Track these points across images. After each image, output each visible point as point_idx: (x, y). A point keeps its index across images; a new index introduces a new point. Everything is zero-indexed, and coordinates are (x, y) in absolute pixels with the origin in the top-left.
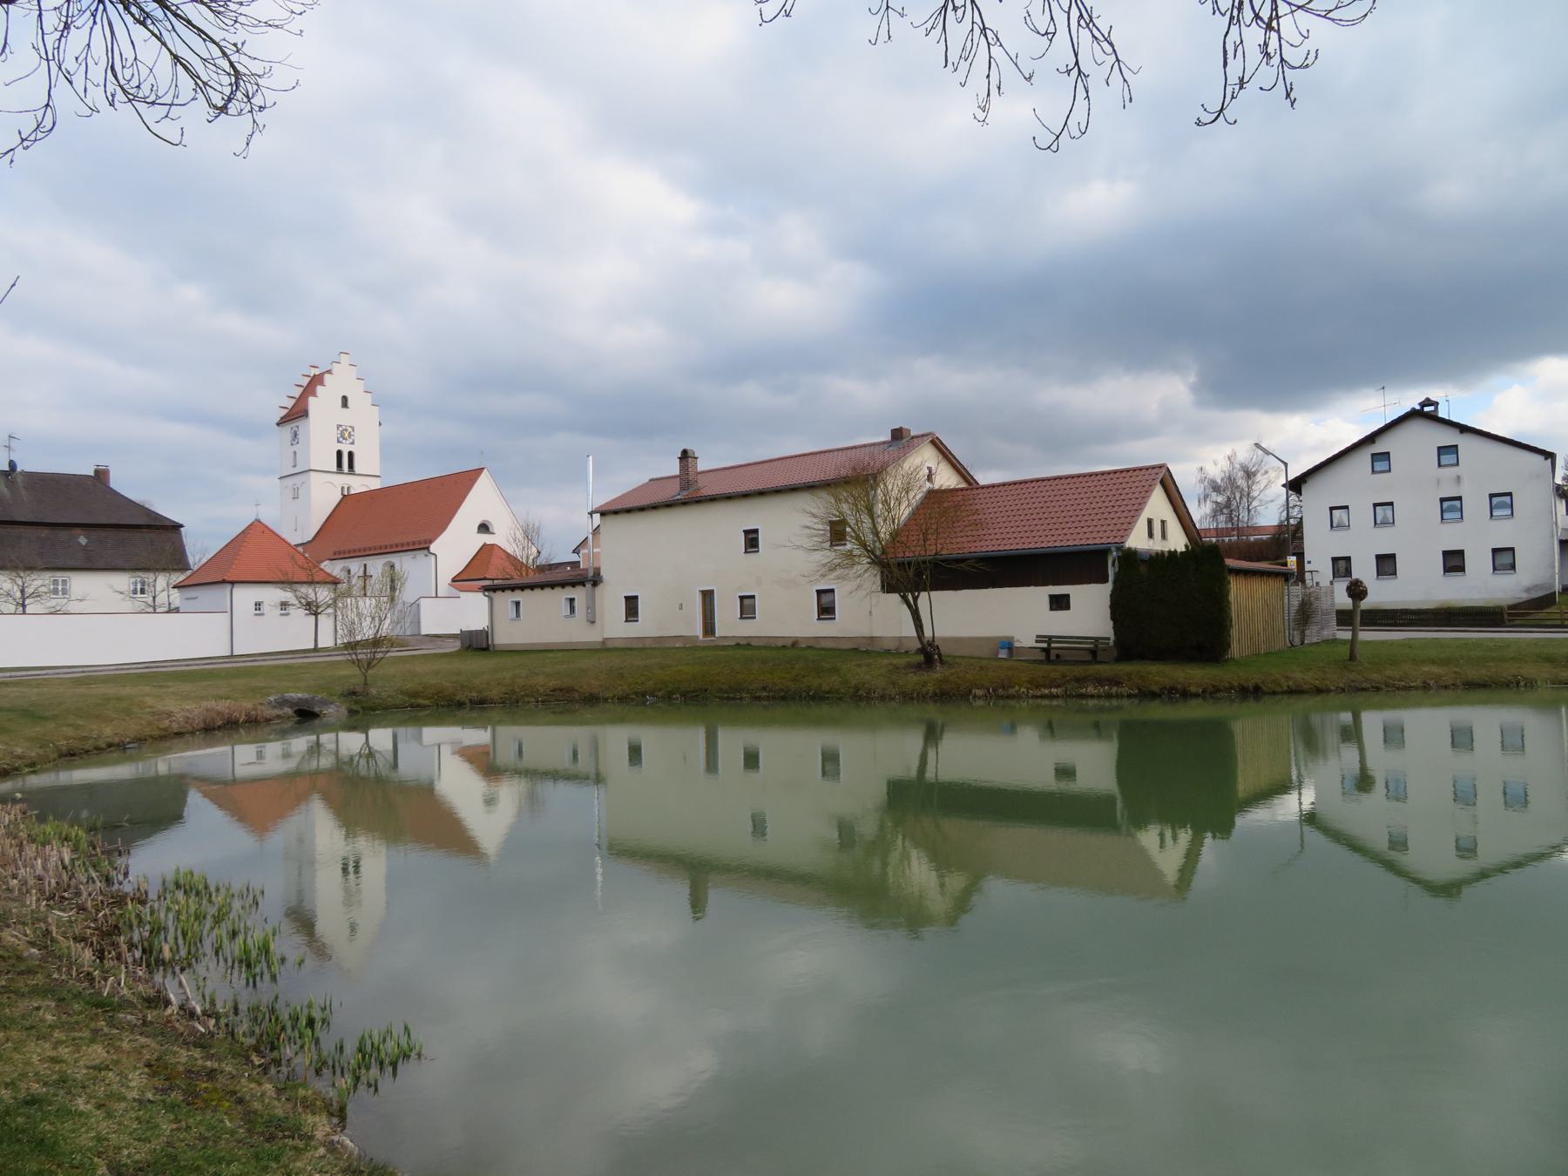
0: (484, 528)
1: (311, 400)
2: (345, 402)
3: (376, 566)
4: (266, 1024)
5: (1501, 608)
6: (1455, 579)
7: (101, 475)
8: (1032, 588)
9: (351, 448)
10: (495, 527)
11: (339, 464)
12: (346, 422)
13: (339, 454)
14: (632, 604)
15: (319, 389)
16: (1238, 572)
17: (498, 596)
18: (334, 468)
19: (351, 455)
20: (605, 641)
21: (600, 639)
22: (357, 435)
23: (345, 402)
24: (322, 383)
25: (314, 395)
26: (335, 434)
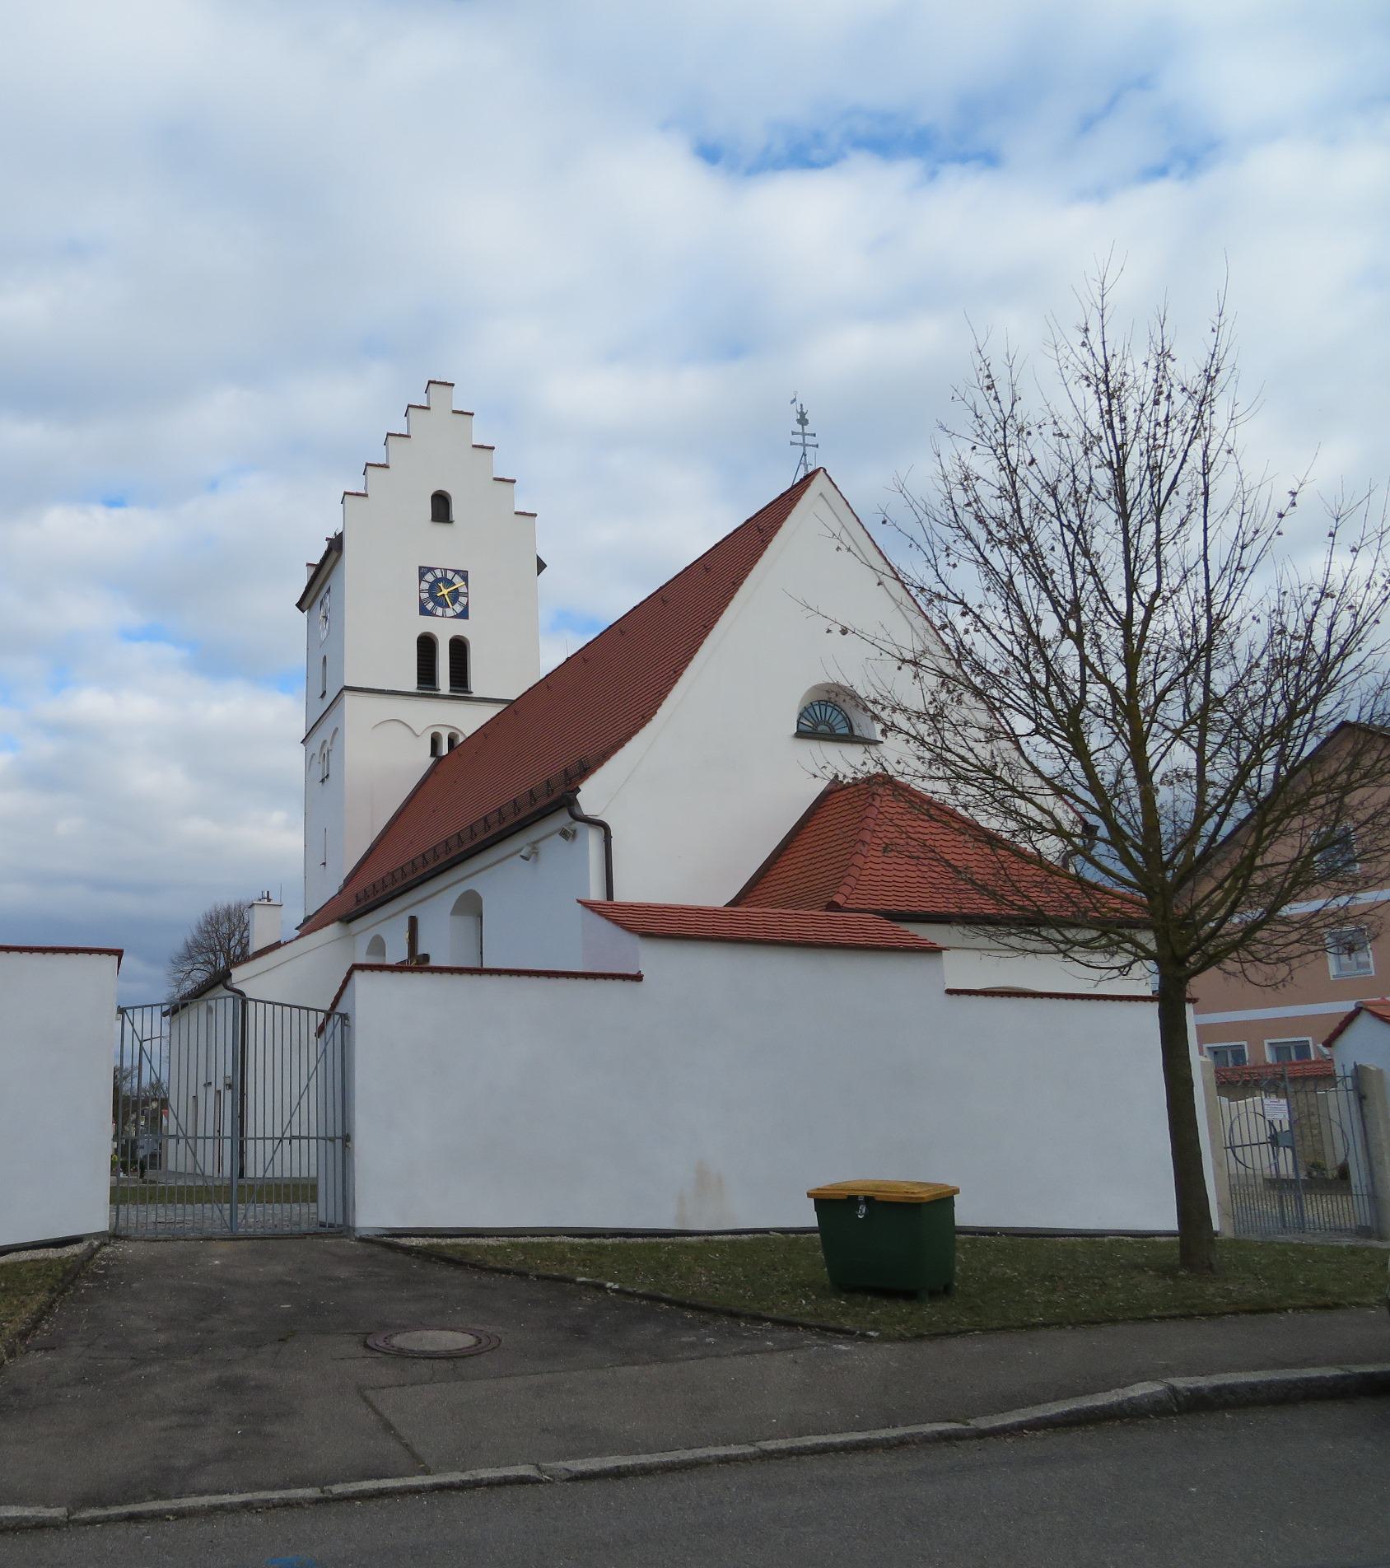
2: (441, 507)
7: (944, 1202)
12: (445, 560)
13: (426, 645)
18: (411, 683)
19: (459, 648)
22: (477, 595)
23: (441, 507)
26: (412, 591)
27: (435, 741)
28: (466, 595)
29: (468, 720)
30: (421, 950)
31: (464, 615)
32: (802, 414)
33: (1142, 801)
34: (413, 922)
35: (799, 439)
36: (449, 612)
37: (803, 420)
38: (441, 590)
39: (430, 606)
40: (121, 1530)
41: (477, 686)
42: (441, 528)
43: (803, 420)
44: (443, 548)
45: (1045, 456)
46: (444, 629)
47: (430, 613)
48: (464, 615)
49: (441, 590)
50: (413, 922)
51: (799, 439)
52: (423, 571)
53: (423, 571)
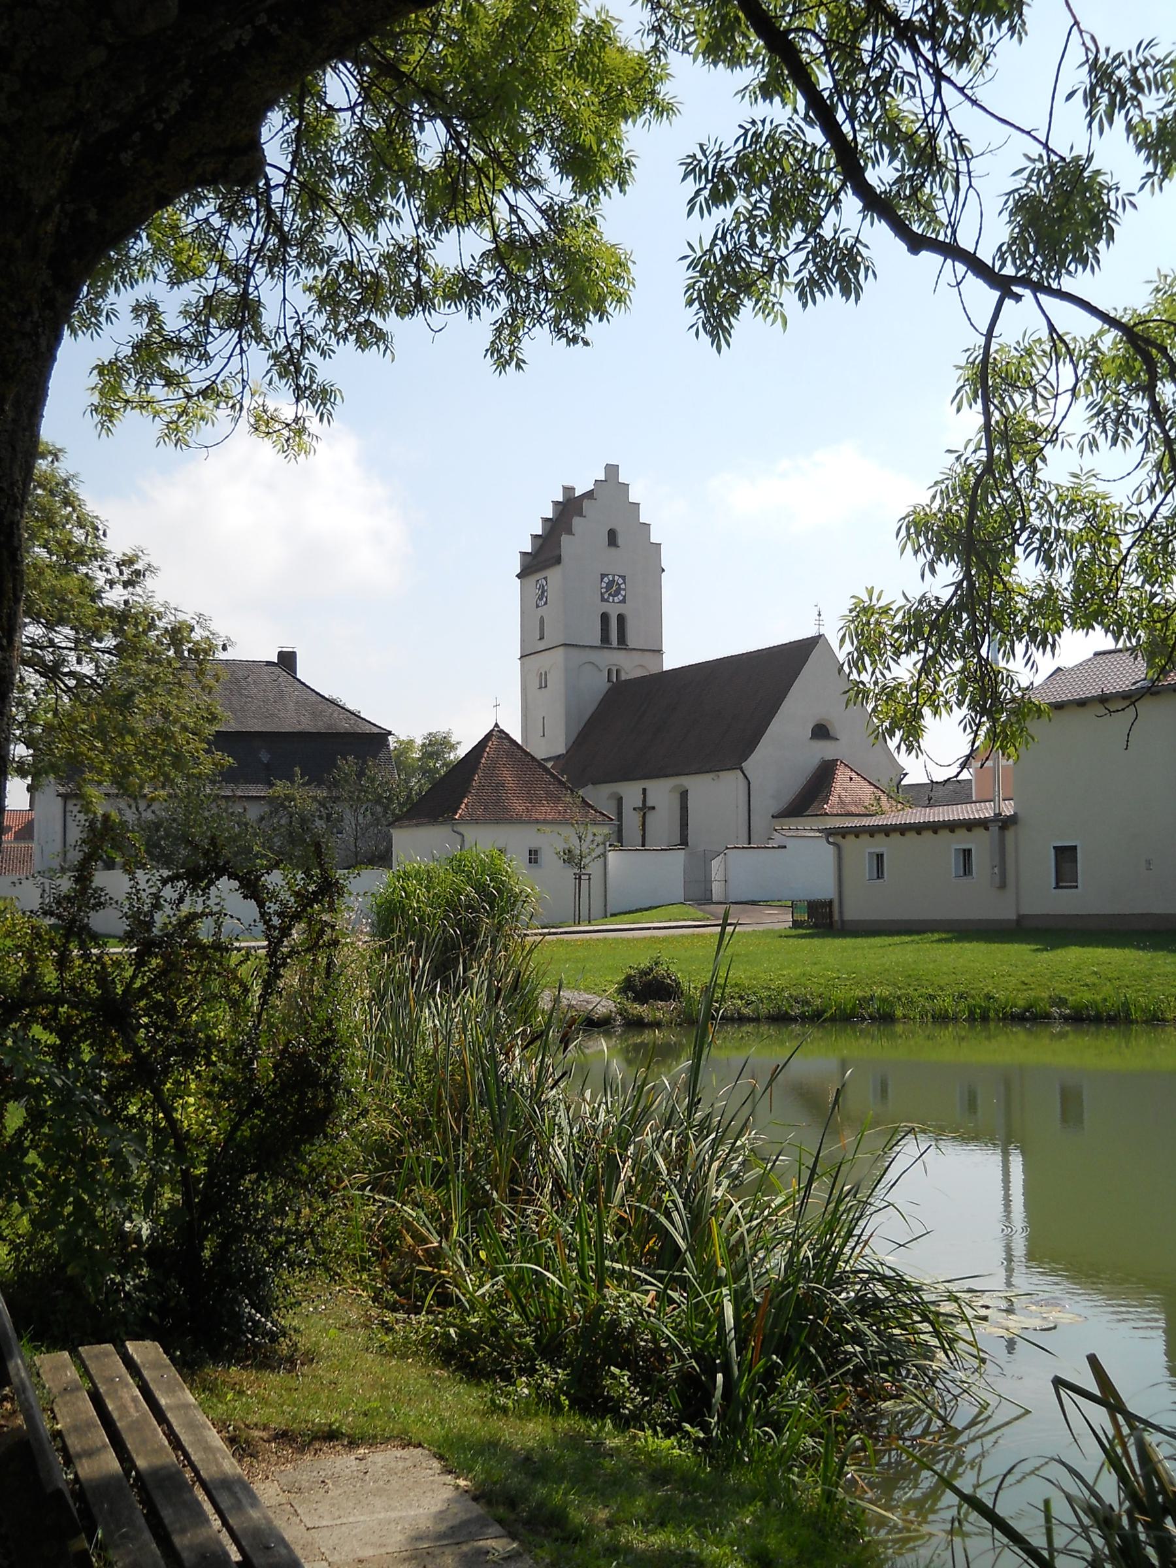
0: (821, 732)
1: (565, 539)
3: (661, 792)
4: (606, 1534)
5: (371, 741)
6: (534, 846)
8: (972, 918)
9: (621, 608)
10: (836, 729)
11: (605, 639)
13: (605, 618)
14: (1066, 856)
15: (577, 521)
16: (841, 913)
17: (849, 843)
18: (598, 643)
19: (621, 619)
20: (1021, 918)
21: (1013, 916)
24: (580, 514)
25: (570, 532)
27: (609, 671)
30: (649, 803)
34: (644, 790)
38: (612, 588)
41: (632, 641)
42: (613, 549)
44: (615, 562)
46: (614, 611)
48: (624, 601)
49: (612, 588)
53: (603, 576)
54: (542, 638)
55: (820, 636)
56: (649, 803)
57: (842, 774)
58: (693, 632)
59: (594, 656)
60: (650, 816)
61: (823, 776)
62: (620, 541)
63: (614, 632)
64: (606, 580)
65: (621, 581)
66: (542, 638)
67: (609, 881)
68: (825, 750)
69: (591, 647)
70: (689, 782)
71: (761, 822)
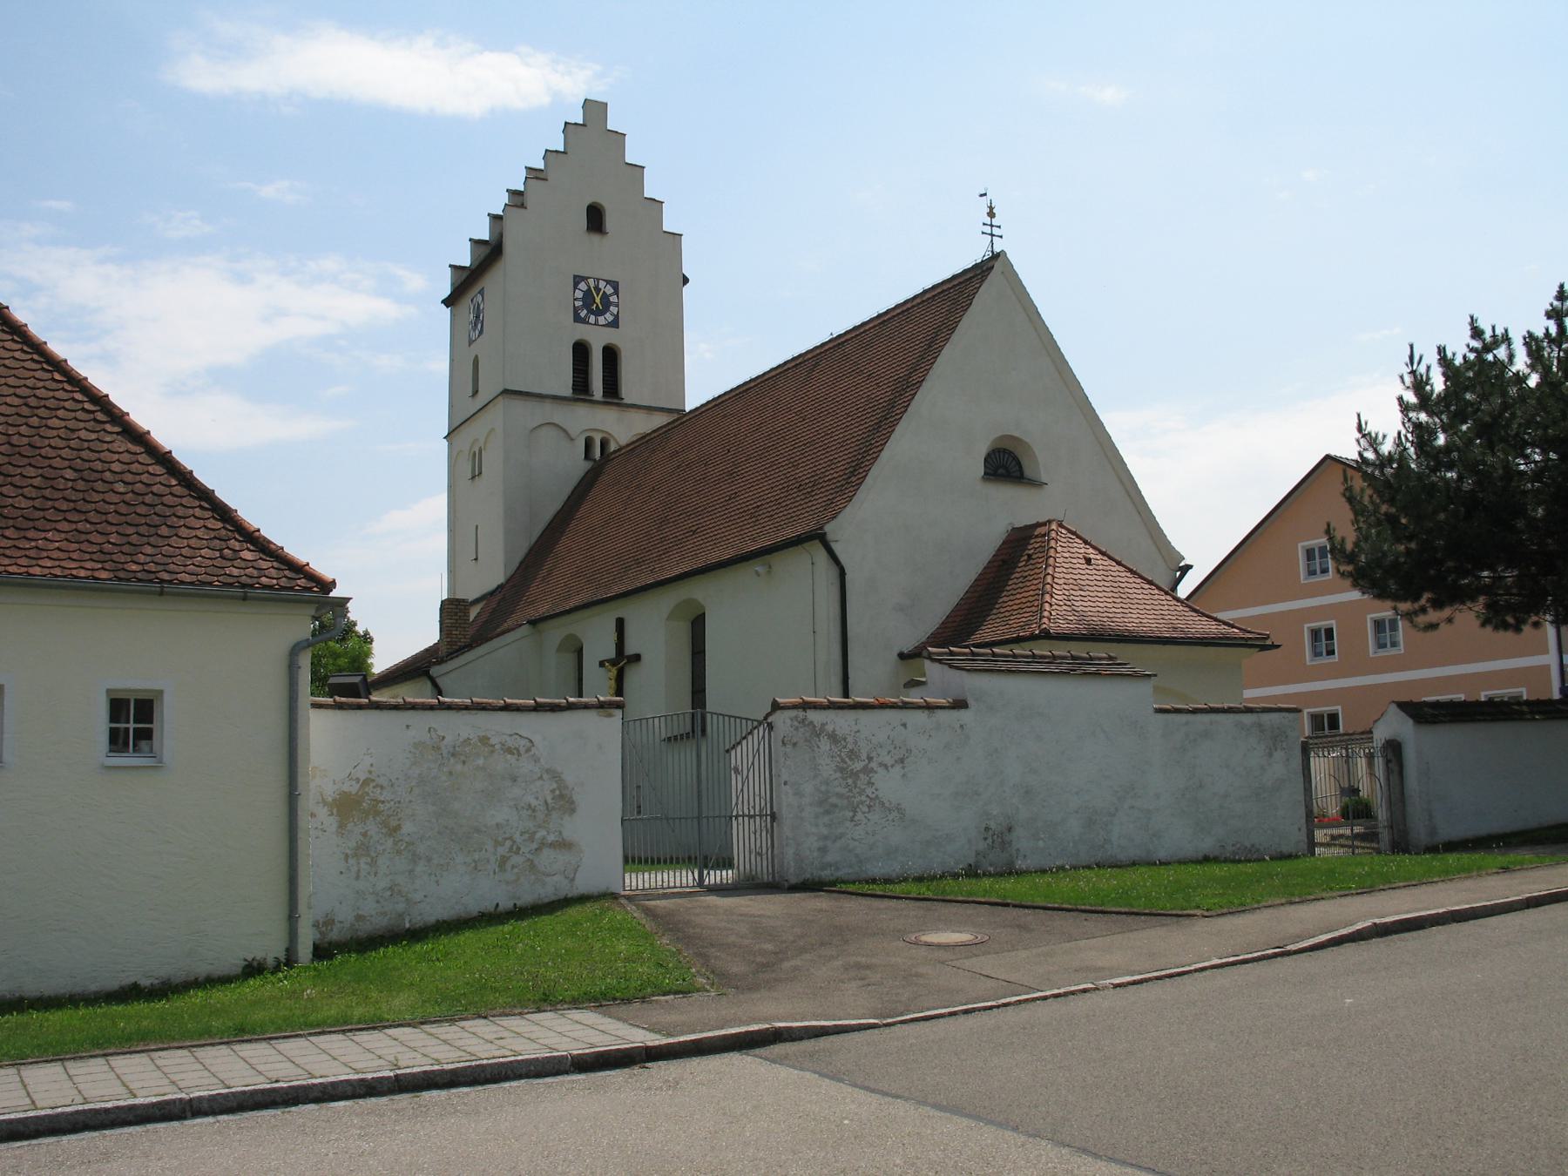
0: (1005, 465)
10: (1043, 462)
13: (581, 352)
18: (568, 392)
19: (611, 355)
22: (625, 305)
26: (570, 298)
27: (589, 443)
28: (617, 305)
29: (622, 428)
30: (630, 650)
31: (615, 324)
32: (991, 208)
33: (1405, 600)
34: (620, 624)
35: (988, 229)
36: (601, 320)
37: (991, 214)
38: (594, 302)
39: (583, 313)
40: (961, 1018)
41: (628, 392)
42: (596, 238)
43: (991, 214)
44: (600, 259)
45: (1387, 448)
46: (598, 339)
47: (584, 321)
48: (615, 324)
49: (594, 302)
50: (620, 624)
51: (988, 229)
52: (578, 280)
53: (578, 280)
54: (475, 392)
55: (996, 256)
56: (630, 650)
57: (1066, 556)
58: (723, 346)
59: (561, 414)
60: (633, 677)
61: (1019, 552)
62: (610, 222)
63: (596, 374)
64: (583, 286)
65: (609, 290)
66: (475, 392)
67: (305, 888)
68: (1013, 507)
69: (555, 398)
70: (703, 592)
71: (873, 674)
